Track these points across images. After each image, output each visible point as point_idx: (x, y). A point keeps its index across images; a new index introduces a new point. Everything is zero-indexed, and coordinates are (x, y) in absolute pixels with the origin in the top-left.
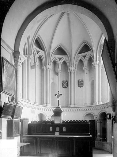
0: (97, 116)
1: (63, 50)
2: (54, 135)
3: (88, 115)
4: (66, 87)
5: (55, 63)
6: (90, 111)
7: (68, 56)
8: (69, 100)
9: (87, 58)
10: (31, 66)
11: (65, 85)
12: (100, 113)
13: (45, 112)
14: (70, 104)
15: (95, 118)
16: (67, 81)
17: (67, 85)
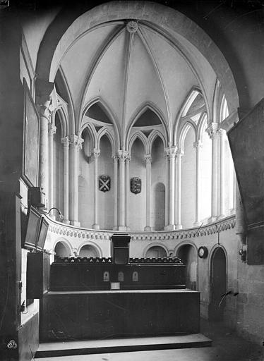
0: (174, 251)
1: (102, 111)
2: (110, 289)
3: (153, 248)
4: (107, 190)
5: (86, 134)
6: (153, 242)
7: (113, 126)
8: (113, 217)
9: (152, 137)
10: (181, 118)
11: (105, 184)
12: (180, 245)
13: (69, 238)
14: (116, 224)
15: (168, 255)
16: (109, 178)
17: (109, 184)
